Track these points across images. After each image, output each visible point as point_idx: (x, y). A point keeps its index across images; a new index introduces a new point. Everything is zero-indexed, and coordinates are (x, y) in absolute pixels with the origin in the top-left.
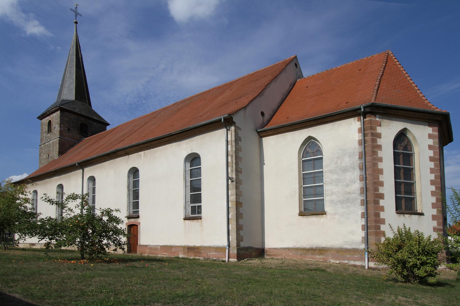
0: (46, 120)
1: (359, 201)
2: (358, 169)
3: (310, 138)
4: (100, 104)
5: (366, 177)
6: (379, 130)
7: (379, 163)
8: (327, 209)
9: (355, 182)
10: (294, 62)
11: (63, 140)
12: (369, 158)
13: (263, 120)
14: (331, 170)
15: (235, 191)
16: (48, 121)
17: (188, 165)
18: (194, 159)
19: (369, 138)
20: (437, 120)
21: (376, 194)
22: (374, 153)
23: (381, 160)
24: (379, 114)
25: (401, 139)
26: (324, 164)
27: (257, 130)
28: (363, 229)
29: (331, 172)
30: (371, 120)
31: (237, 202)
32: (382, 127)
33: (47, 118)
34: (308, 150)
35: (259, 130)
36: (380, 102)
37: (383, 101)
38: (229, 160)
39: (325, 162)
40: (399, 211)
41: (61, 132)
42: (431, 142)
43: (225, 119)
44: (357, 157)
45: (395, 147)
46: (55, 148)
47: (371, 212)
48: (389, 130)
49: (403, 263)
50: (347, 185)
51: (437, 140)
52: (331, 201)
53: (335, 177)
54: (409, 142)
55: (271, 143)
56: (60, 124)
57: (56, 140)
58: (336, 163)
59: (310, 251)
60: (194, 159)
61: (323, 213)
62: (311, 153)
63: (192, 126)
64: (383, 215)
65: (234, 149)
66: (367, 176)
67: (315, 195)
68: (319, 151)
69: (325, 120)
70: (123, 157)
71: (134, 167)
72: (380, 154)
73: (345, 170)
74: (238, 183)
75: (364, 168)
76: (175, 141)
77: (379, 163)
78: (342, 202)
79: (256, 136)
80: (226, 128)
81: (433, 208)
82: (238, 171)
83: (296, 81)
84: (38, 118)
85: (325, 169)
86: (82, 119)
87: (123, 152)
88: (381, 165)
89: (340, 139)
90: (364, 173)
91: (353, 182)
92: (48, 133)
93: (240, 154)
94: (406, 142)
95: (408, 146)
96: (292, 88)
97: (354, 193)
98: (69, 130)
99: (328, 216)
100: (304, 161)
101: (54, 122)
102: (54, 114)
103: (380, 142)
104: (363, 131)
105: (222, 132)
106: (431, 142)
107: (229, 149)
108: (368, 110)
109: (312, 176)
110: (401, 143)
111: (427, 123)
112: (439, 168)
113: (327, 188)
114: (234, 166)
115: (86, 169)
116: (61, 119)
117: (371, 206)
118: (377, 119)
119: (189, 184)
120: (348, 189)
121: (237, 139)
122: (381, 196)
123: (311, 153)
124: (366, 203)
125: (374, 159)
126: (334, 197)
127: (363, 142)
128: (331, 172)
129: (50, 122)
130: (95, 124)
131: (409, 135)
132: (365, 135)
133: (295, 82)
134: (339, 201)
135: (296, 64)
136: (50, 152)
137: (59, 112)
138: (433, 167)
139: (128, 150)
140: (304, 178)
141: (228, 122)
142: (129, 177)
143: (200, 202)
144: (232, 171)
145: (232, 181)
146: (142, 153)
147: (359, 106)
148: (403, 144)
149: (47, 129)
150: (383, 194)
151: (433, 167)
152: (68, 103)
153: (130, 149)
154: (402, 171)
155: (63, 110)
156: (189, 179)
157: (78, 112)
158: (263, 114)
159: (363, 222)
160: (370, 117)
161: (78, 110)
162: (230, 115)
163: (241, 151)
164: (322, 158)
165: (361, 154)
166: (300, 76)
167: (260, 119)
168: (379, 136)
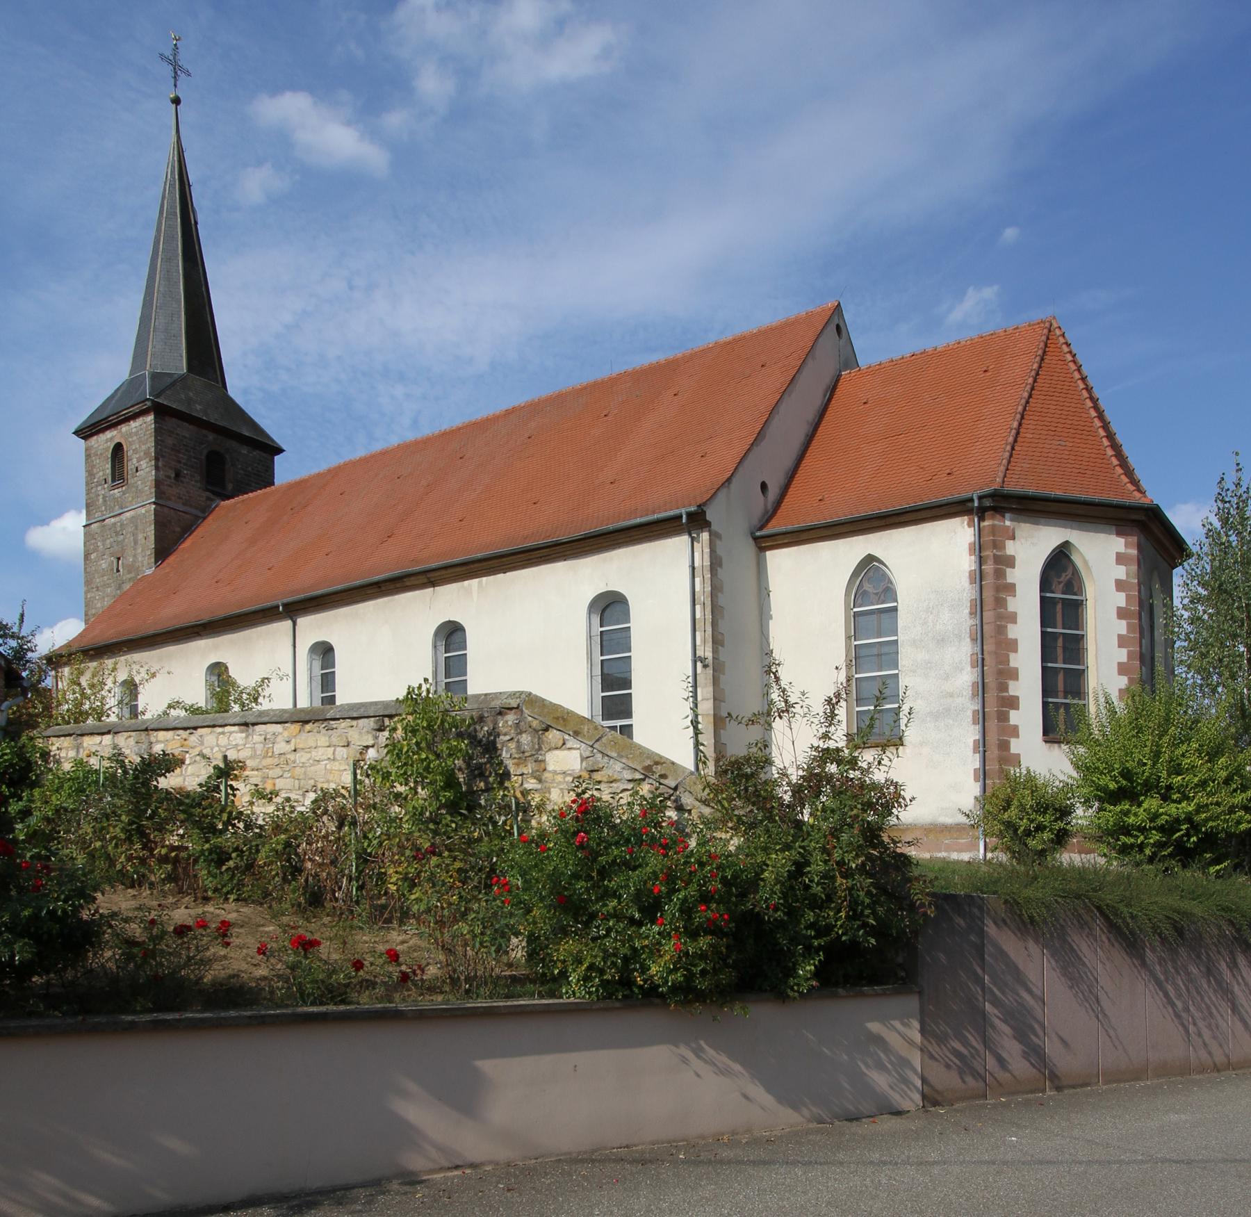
0: (105, 441)
1: (970, 713)
3: (870, 559)
6: (1011, 548)
7: (1010, 626)
10: (835, 323)
11: (166, 510)
12: (988, 615)
13: (766, 506)
14: (914, 641)
15: (711, 689)
17: (596, 620)
18: (610, 606)
19: (989, 568)
20: (1133, 521)
21: (1003, 698)
22: (1000, 603)
24: (1010, 510)
25: (1059, 566)
26: (901, 623)
27: (752, 534)
28: (976, 780)
30: (993, 526)
31: (715, 715)
33: (109, 434)
34: (867, 587)
35: (758, 534)
36: (1013, 487)
37: (1019, 485)
38: (698, 615)
39: (903, 619)
40: (1051, 736)
41: (158, 484)
42: (1121, 572)
43: (689, 515)
44: (967, 611)
45: (1045, 584)
46: (140, 536)
47: (992, 738)
48: (1031, 546)
49: (1010, 825)
50: (947, 677)
51: (1134, 568)
54: (1076, 572)
55: (781, 562)
56: (157, 459)
57: (143, 511)
60: (610, 606)
63: (611, 527)
64: (1015, 746)
65: (708, 589)
66: (986, 656)
68: (889, 592)
69: (902, 519)
70: (417, 593)
71: (450, 622)
72: (1013, 604)
73: (943, 640)
74: (718, 668)
75: (979, 637)
76: (564, 557)
79: (749, 548)
80: (690, 535)
81: (1016, 728)
82: (717, 642)
83: (840, 376)
84: (77, 433)
85: (902, 637)
86: (211, 436)
87: (423, 579)
88: (1013, 632)
89: (932, 562)
90: (979, 649)
92: (113, 488)
93: (722, 601)
94: (1070, 572)
95: (1074, 584)
96: (830, 400)
98: (178, 475)
101: (135, 451)
102: (134, 424)
103: (1013, 576)
104: (979, 549)
105: (680, 543)
106: (1121, 572)
107: (698, 588)
108: (987, 503)
109: (875, 651)
110: (1060, 577)
111: (1114, 528)
112: (1138, 635)
114: (709, 629)
115: (302, 621)
116: (158, 443)
117: (992, 724)
118: (1008, 523)
121: (716, 563)
122: (1013, 703)
124: (982, 718)
127: (979, 577)
129: (118, 448)
131: (1075, 558)
132: (981, 561)
133: (837, 381)
135: (838, 327)
136: (123, 551)
137: (150, 418)
138: (1124, 632)
139: (438, 574)
141: (696, 522)
142: (435, 647)
144: (705, 642)
145: (705, 666)
147: (968, 495)
148: (1064, 577)
149: (109, 471)
150: (1017, 698)
151: (1124, 632)
152: (173, 384)
153: (443, 572)
154: (1060, 642)
155: (161, 412)
157: (200, 415)
158: (764, 486)
159: (976, 762)
160: (993, 518)
161: (198, 407)
162: (699, 506)
163: (721, 591)
164: (895, 609)
166: (850, 361)
167: (759, 504)
168: (1010, 562)
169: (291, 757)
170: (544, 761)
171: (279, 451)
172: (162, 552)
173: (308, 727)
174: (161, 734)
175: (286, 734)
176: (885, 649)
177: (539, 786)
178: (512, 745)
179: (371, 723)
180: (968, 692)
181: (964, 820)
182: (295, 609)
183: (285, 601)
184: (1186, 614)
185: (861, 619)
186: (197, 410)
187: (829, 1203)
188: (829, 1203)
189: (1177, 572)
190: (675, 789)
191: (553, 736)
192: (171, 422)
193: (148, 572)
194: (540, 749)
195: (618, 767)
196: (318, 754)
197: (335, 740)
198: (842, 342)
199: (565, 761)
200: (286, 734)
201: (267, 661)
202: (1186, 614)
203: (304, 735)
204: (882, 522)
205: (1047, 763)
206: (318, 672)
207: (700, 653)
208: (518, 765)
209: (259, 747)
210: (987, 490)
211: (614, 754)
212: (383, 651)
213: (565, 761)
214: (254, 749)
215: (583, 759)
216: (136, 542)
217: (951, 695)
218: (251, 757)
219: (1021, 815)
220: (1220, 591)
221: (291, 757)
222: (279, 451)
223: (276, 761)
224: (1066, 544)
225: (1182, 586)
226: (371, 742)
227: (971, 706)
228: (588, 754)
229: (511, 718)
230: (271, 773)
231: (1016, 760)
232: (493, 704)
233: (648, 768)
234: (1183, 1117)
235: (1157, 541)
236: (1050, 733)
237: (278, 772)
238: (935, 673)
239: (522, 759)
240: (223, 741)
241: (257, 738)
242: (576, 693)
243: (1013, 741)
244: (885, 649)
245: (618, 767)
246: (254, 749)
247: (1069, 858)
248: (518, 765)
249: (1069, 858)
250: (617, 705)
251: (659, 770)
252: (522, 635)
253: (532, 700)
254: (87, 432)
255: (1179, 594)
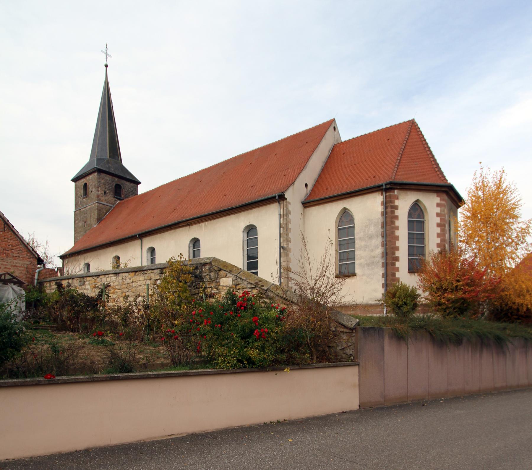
1: (381, 264)
2: (380, 237)
4: (131, 160)
5: (386, 244)
6: (397, 203)
8: (357, 271)
9: (378, 248)
16: (83, 184)
17: (246, 235)
18: (251, 230)
23: (397, 228)
25: (417, 209)
28: (383, 287)
29: (360, 239)
32: (399, 200)
33: (82, 180)
39: (357, 230)
42: (438, 210)
44: (380, 226)
46: (92, 214)
47: (389, 272)
48: (404, 202)
50: (372, 250)
52: (360, 265)
53: (363, 243)
58: (365, 231)
59: (344, 309)
60: (251, 230)
61: (354, 275)
62: (345, 223)
64: (398, 275)
66: (388, 243)
67: (348, 259)
68: (352, 221)
69: (357, 194)
72: (397, 223)
76: (234, 213)
77: (396, 231)
78: (368, 265)
85: (356, 237)
86: (116, 179)
91: (377, 247)
97: (377, 257)
98: (105, 193)
99: (358, 278)
100: (339, 230)
101: (91, 185)
102: (91, 176)
103: (397, 213)
106: (438, 210)
108: (388, 186)
109: (346, 242)
113: (357, 253)
119: (246, 253)
120: (373, 254)
123: (345, 223)
125: (393, 228)
126: (362, 261)
127: (385, 214)
128: (360, 239)
129: (86, 185)
130: (128, 183)
132: (386, 208)
134: (366, 264)
135: (334, 128)
137: (96, 174)
140: (340, 245)
143: (257, 269)
146: (203, 224)
149: (82, 193)
156: (246, 248)
159: (382, 281)
164: (354, 227)
165: (383, 223)
168: (396, 208)
169: (131, 284)
170: (219, 282)
171: (140, 183)
172: (99, 220)
173: (137, 274)
174: (88, 279)
175: (129, 276)
176: (350, 241)
177: (217, 291)
178: (208, 277)
179: (158, 271)
180: (380, 256)
181: (378, 302)
182: (142, 236)
183: (139, 233)
184: (462, 223)
185: (341, 231)
186: (112, 170)
187: (318, 449)
188: (318, 449)
189: (459, 210)
190: (267, 290)
191: (222, 273)
192: (103, 175)
193: (95, 226)
194: (218, 277)
195: (246, 283)
196: (140, 283)
197: (146, 278)
198: (336, 133)
199: (227, 282)
200: (129, 276)
201: (133, 256)
202: (462, 223)
203: (136, 277)
204: (349, 196)
205: (408, 280)
206: (150, 258)
207: (282, 245)
208: (209, 284)
209: (121, 281)
210: (388, 181)
211: (244, 278)
212: (172, 248)
213: (227, 282)
214: (119, 282)
215: (233, 280)
216: (91, 216)
217: (374, 257)
218: (118, 285)
219: (399, 300)
220: (474, 216)
221: (131, 284)
222: (140, 183)
223: (126, 286)
224: (418, 201)
225: (462, 213)
226: (158, 278)
227: (381, 261)
228: (235, 279)
229: (207, 267)
230: (124, 290)
231: (398, 280)
232: (201, 262)
233: (257, 283)
234: (462, 412)
235: (453, 198)
236: (412, 270)
237: (127, 290)
238: (368, 249)
239: (211, 281)
240: (108, 280)
241: (120, 278)
242: (238, 260)
243: (397, 273)
244: (350, 241)
245: (246, 283)
246: (119, 282)
247: (418, 314)
248: (209, 284)
249: (418, 314)
250: (253, 265)
251: (261, 284)
252: (222, 241)
253: (215, 260)
254: (75, 180)
255: (460, 217)
